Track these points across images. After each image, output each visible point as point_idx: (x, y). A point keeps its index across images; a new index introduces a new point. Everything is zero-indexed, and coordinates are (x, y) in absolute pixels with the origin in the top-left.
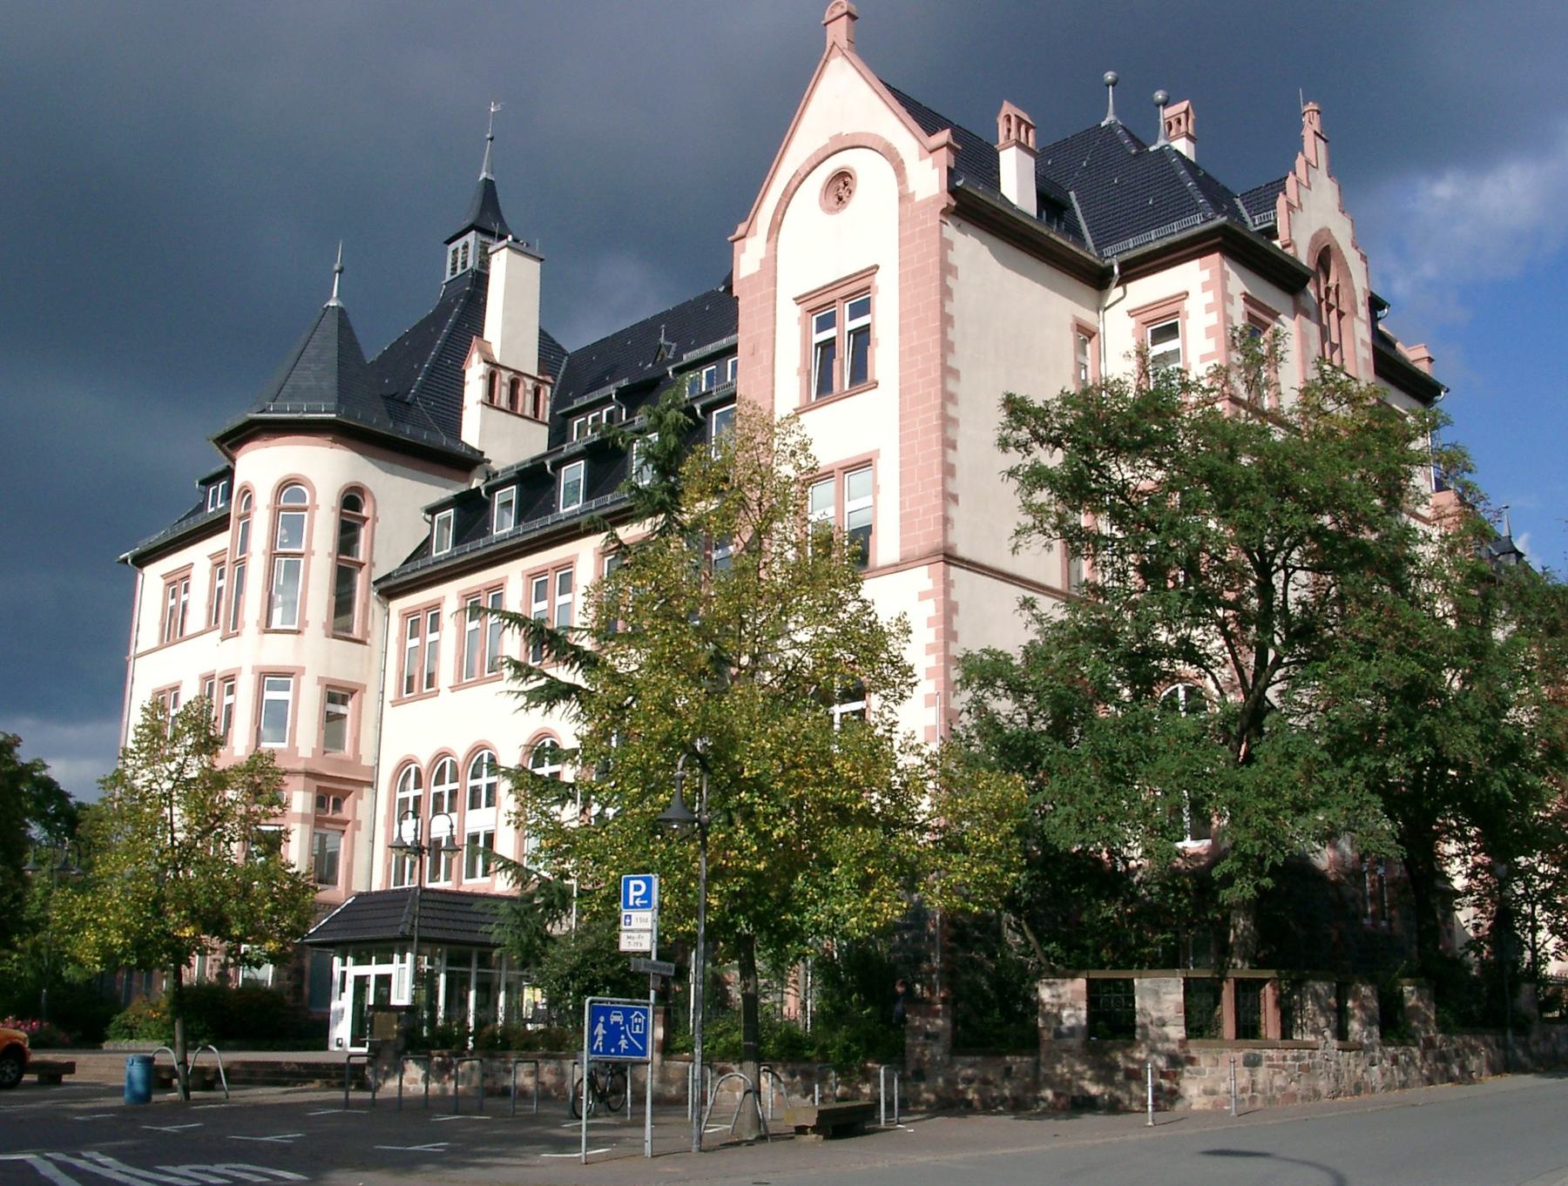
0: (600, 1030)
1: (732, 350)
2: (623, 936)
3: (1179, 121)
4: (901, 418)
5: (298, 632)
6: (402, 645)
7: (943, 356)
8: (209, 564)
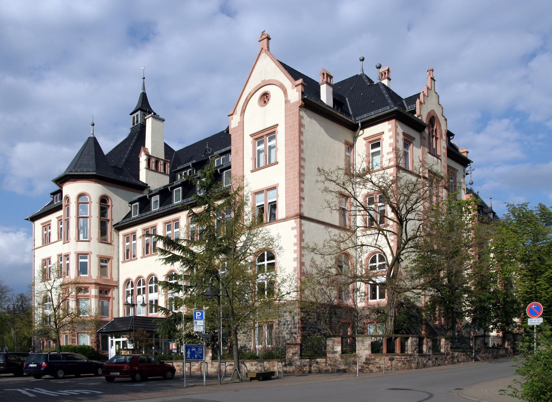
0: (189, 353)
1: (229, 151)
2: (195, 327)
3: (385, 73)
4: (286, 173)
5: (89, 241)
6: (124, 245)
7: (300, 154)
8: (56, 220)
